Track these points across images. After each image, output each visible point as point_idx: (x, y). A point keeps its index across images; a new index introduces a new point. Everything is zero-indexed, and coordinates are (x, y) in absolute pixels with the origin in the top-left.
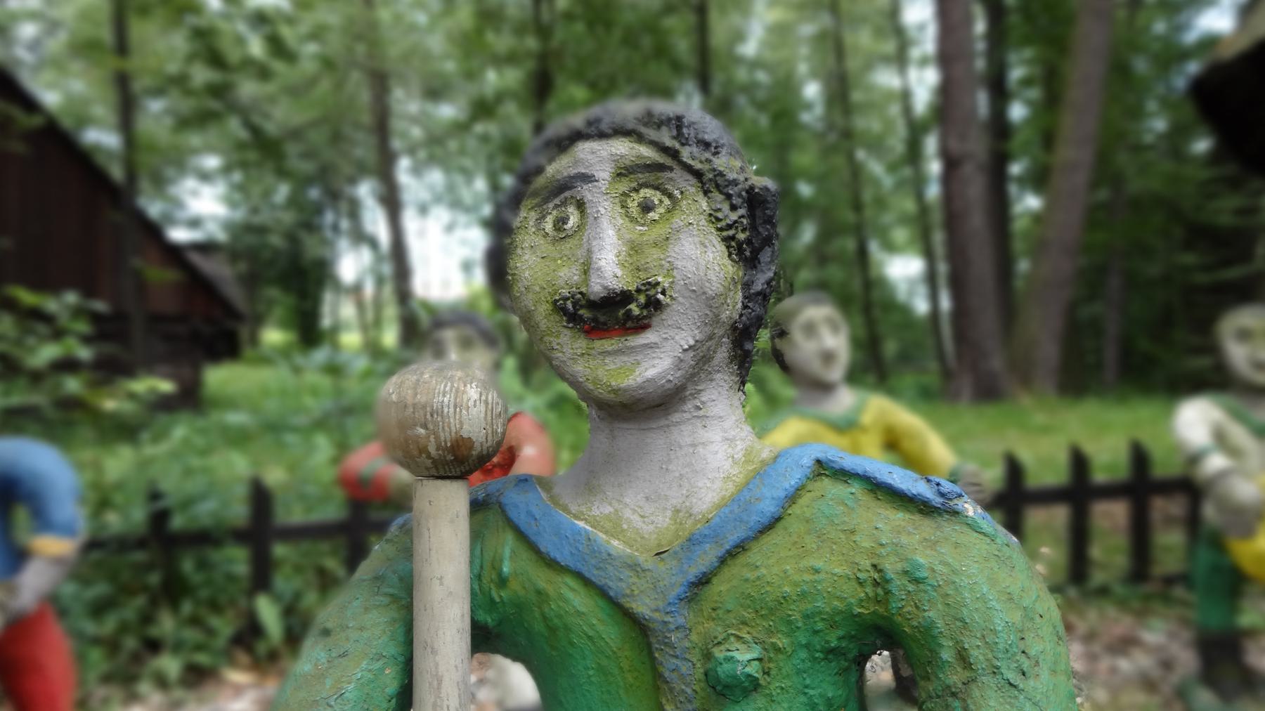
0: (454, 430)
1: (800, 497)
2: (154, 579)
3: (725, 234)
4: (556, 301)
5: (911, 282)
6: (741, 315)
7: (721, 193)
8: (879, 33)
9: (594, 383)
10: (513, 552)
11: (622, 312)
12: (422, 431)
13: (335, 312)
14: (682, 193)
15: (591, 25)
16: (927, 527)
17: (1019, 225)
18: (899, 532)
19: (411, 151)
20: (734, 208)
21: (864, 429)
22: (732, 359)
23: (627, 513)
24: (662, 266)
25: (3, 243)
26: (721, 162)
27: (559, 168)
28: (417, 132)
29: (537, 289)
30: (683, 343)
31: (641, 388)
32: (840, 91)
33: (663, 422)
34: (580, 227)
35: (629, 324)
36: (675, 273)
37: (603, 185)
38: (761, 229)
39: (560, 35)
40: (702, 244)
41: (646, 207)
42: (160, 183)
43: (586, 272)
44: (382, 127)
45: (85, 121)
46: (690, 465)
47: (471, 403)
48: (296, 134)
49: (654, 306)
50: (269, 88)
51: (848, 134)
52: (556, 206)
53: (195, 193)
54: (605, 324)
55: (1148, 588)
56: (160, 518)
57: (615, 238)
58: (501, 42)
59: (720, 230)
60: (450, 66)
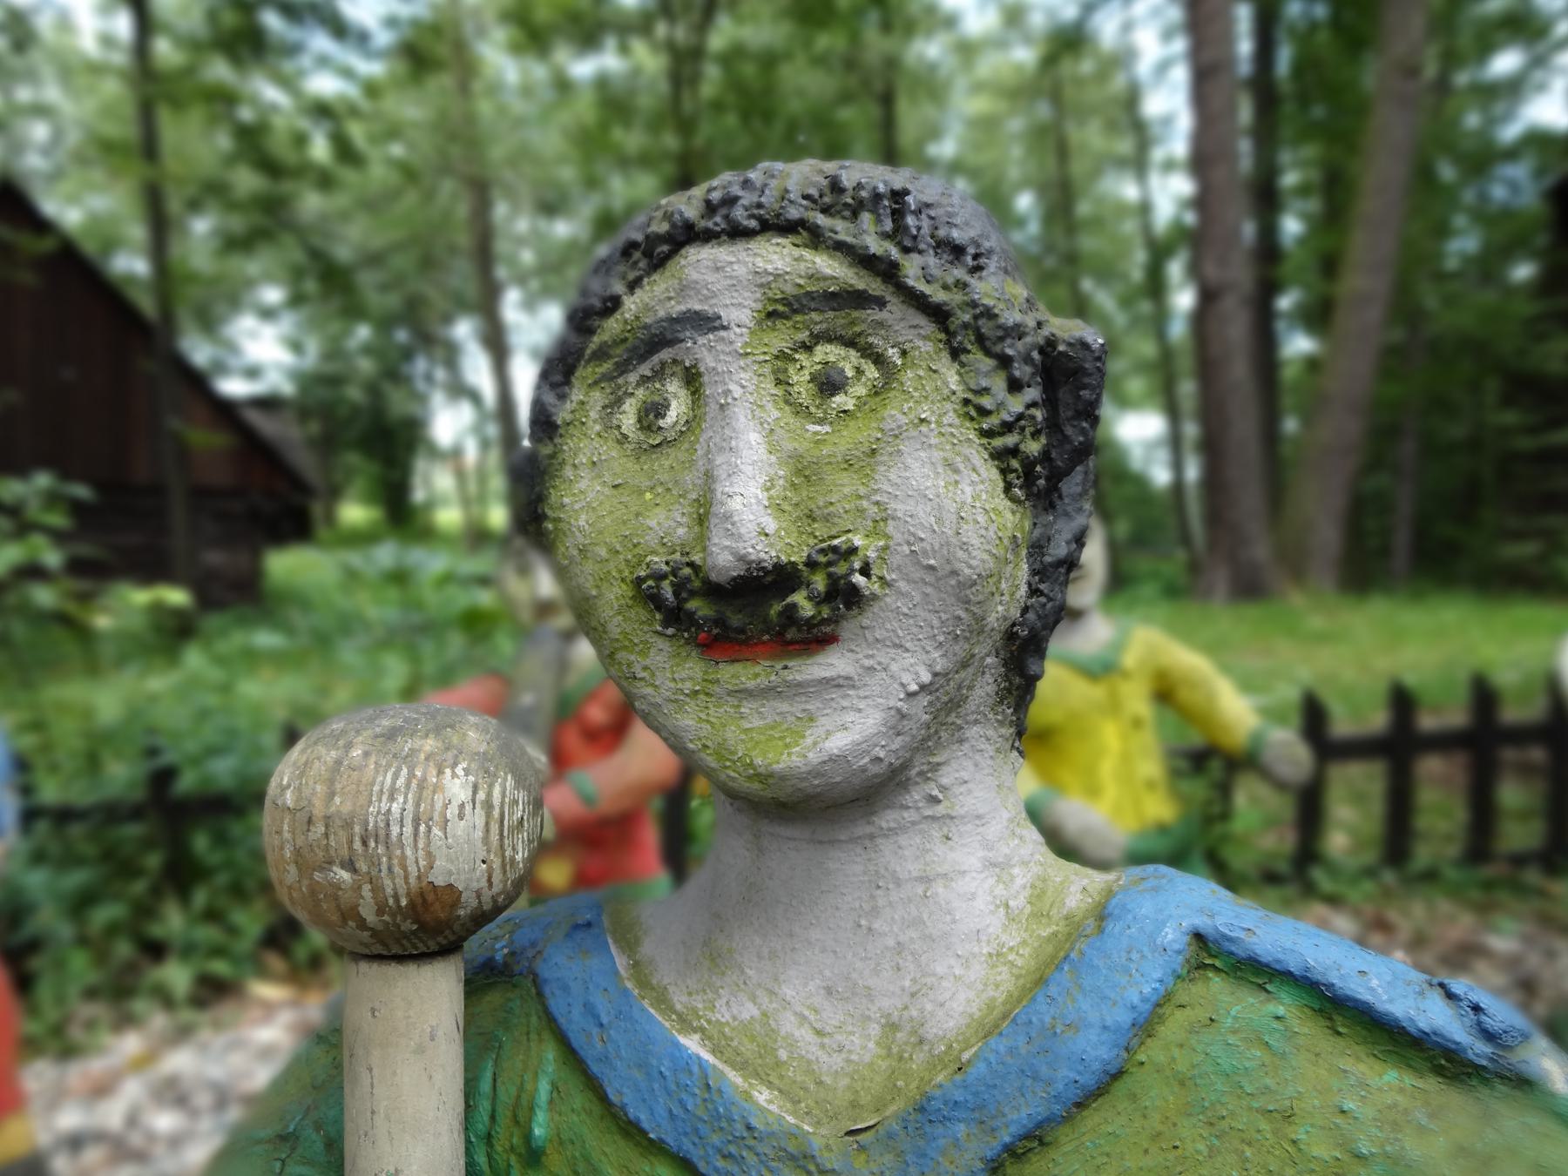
0: (413, 869)
1: (1161, 1019)
2: (154, 861)
3: (998, 442)
4: (639, 581)
5: (1151, 446)
6: (1025, 610)
7: (988, 353)
8: (1111, 127)
9: (719, 755)
10: (555, 1087)
11: (776, 608)
12: (345, 875)
13: (428, 483)
14: (904, 353)
15: (745, 117)
16: (1455, 1102)
17: (1289, 374)
18: (1396, 1126)
19: (521, 280)
20: (1015, 386)
21: (1125, 675)
22: (1001, 697)
23: (788, 1024)
24: (861, 511)
25: (6, 397)
26: (986, 288)
27: (650, 301)
28: (527, 257)
29: (603, 552)
30: (906, 678)
31: (818, 775)
32: (1061, 200)
33: (862, 829)
34: (692, 423)
35: (790, 634)
36: (890, 528)
37: (738, 337)
38: (1069, 431)
39: (705, 131)
40: (950, 466)
41: (828, 384)
42: (209, 324)
43: (701, 520)
44: (484, 254)
45: (111, 244)
46: (918, 922)
47: (452, 812)
48: (375, 259)
49: (844, 597)
50: (340, 200)
51: (1072, 259)
52: (644, 380)
53: (253, 335)
54: (742, 631)
55: (1488, 871)
56: (163, 778)
57: (762, 450)
58: (632, 139)
59: (988, 434)
60: (568, 174)
